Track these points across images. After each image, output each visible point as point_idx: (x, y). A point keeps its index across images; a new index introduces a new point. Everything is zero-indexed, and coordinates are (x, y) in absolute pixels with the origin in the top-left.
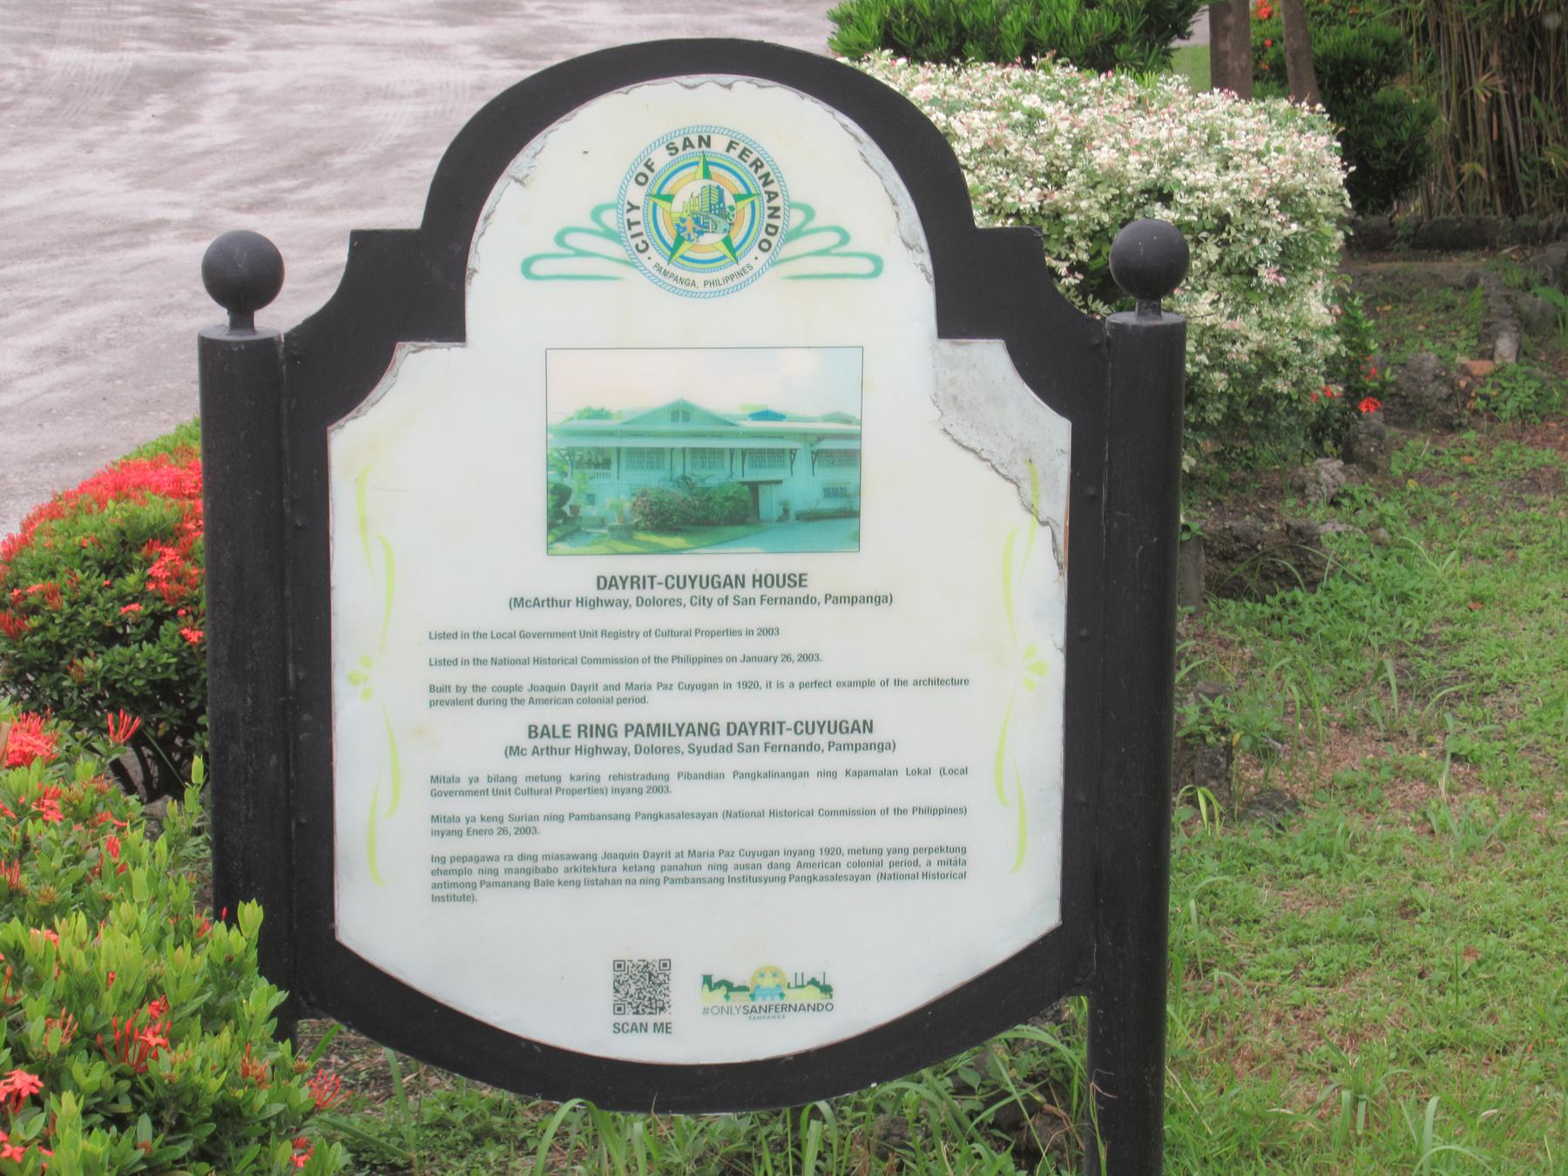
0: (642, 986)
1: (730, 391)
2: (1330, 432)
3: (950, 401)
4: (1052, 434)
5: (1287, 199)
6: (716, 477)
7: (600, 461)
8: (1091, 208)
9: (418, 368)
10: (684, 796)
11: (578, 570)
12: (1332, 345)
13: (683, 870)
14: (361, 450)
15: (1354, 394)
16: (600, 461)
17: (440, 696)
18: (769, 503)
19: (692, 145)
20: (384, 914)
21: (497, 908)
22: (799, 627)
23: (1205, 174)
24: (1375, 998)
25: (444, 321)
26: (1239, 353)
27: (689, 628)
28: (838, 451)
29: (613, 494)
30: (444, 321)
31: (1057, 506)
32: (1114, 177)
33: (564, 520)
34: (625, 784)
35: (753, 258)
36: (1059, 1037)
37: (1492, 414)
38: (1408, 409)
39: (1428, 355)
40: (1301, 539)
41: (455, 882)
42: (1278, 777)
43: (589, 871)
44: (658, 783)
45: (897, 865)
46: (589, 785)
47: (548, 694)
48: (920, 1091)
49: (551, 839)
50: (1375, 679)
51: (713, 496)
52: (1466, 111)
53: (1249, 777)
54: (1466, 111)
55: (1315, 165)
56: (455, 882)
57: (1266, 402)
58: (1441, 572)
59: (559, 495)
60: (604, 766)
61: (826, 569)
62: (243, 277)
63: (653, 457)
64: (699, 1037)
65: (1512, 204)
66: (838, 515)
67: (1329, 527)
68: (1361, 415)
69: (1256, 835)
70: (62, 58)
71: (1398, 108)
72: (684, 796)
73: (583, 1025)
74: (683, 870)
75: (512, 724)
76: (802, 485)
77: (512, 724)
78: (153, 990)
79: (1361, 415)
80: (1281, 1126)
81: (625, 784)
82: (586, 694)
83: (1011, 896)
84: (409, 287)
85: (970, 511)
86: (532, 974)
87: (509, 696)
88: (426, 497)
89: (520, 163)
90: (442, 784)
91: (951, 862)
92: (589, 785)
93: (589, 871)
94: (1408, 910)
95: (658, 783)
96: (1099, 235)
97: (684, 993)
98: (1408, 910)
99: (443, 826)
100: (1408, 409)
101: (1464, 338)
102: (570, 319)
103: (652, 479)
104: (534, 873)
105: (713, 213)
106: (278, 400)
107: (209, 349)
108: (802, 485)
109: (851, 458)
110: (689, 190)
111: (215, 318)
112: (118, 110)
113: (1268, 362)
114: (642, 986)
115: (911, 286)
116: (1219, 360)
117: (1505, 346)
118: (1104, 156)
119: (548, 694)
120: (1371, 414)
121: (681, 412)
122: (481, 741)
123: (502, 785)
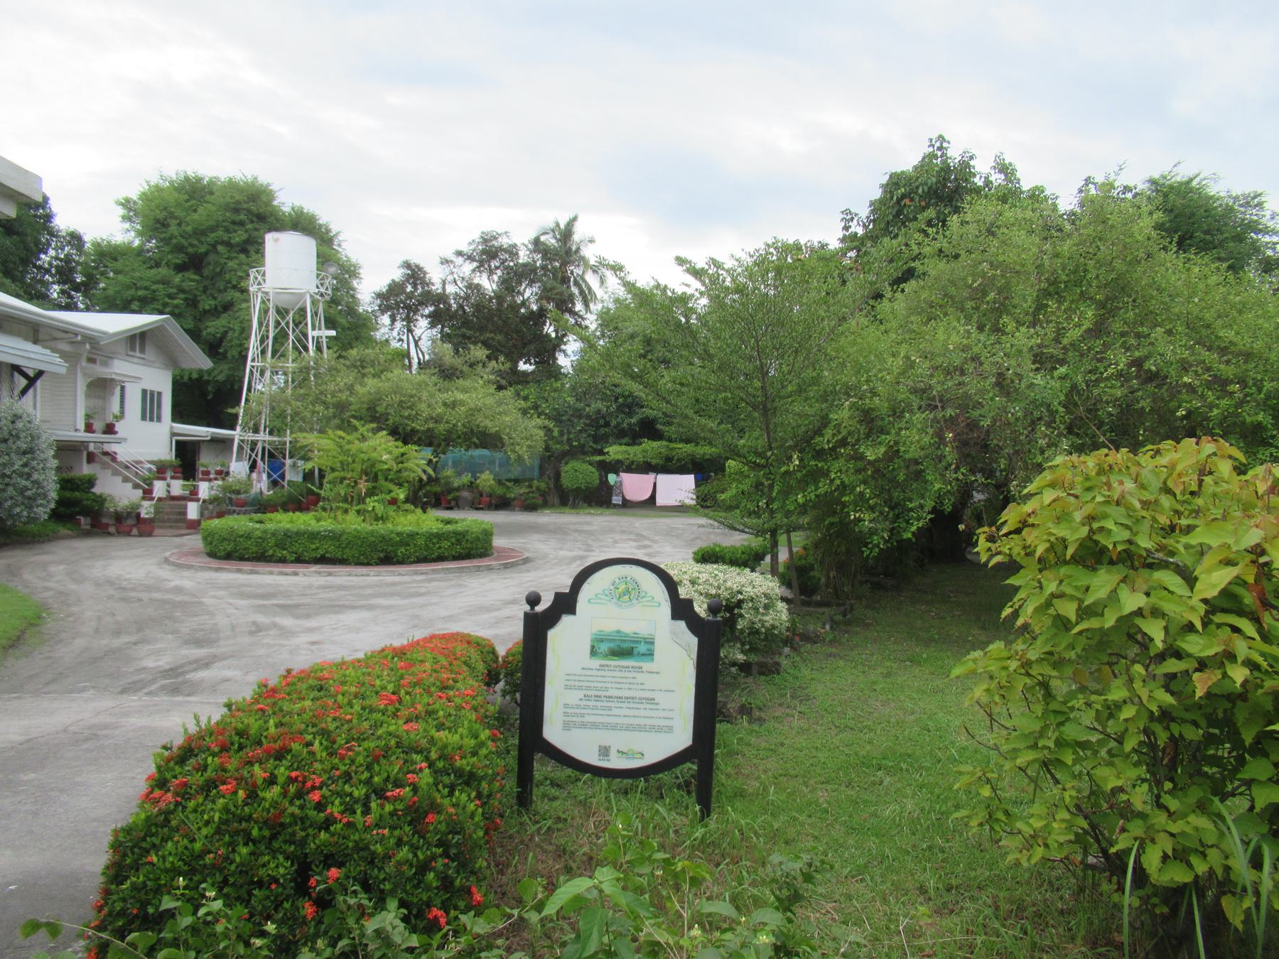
0: (604, 751)
1: (629, 628)
2: (787, 642)
3: (673, 633)
4: (694, 641)
5: (766, 595)
6: (625, 645)
7: (602, 641)
8: (726, 594)
9: (566, 620)
10: (615, 711)
11: (596, 663)
12: (787, 624)
13: (614, 727)
14: (552, 634)
15: (794, 634)
16: (602, 641)
17: (567, 687)
18: (635, 651)
19: (624, 578)
20: (553, 732)
21: (576, 732)
22: (640, 677)
23: (749, 589)
24: (772, 764)
25: (571, 610)
26: (767, 625)
27: (617, 674)
28: (650, 642)
29: (604, 647)
30: (571, 610)
31: (694, 656)
32: (731, 588)
33: (593, 652)
34: (603, 708)
35: (635, 601)
36: (691, 767)
37: (824, 640)
38: (806, 638)
39: (811, 627)
40: (778, 664)
41: (567, 726)
42: (763, 715)
43: (594, 726)
44: (610, 709)
45: (659, 729)
46: (595, 708)
47: (588, 688)
48: (665, 777)
49: (588, 719)
50: (1111, 654)
51: (623, 649)
52: (828, 578)
53: (757, 713)
54: (828, 578)
55: (773, 589)
56: (567, 726)
57: (773, 634)
58: (806, 672)
59: (593, 647)
60: (599, 704)
61: (646, 665)
62: (533, 600)
63: (610, 641)
64: (616, 762)
65: (838, 598)
66: (650, 655)
67: (784, 662)
68: (795, 639)
69: (756, 727)
70: (562, 553)
71: (814, 577)
72: (615, 711)
73: (592, 759)
74: (614, 727)
75: (581, 694)
76: (642, 648)
77: (581, 694)
78: (460, 748)
79: (795, 639)
80: (744, 790)
81: (603, 708)
82: (596, 689)
83: (681, 738)
84: (565, 604)
85: (677, 656)
86: (582, 747)
87: (580, 688)
88: (566, 644)
89: (589, 580)
90: (566, 706)
91: (670, 729)
92: (595, 708)
93: (594, 726)
94: (782, 744)
95: (610, 709)
96: (727, 600)
97: (613, 753)
98: (782, 744)
99: (566, 714)
100: (806, 638)
101: (820, 625)
102: (597, 612)
103: (612, 645)
104: (583, 725)
105: (627, 592)
106: (538, 626)
107: (526, 614)
108: (642, 648)
109: (653, 643)
110: (622, 587)
111: (527, 608)
112: (570, 563)
113: (773, 627)
114: (604, 751)
115: (666, 609)
116: (763, 626)
117: (828, 627)
118: (729, 584)
119: (588, 688)
120: (797, 638)
121: (619, 632)
122: (574, 697)
123: (578, 706)
